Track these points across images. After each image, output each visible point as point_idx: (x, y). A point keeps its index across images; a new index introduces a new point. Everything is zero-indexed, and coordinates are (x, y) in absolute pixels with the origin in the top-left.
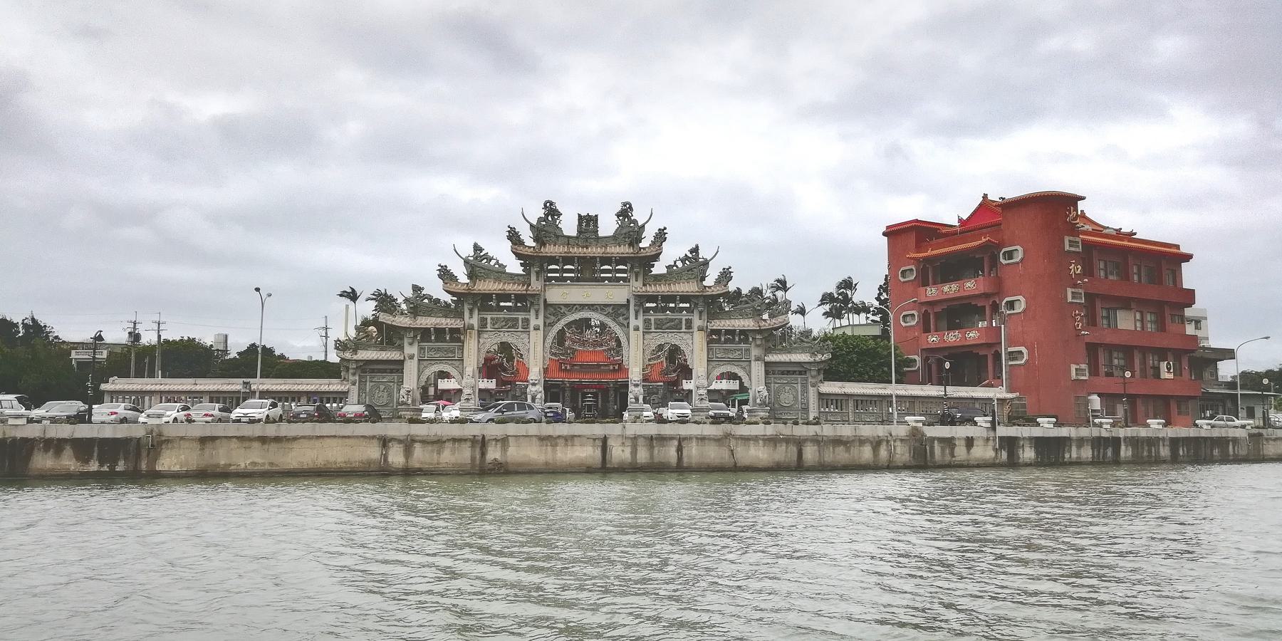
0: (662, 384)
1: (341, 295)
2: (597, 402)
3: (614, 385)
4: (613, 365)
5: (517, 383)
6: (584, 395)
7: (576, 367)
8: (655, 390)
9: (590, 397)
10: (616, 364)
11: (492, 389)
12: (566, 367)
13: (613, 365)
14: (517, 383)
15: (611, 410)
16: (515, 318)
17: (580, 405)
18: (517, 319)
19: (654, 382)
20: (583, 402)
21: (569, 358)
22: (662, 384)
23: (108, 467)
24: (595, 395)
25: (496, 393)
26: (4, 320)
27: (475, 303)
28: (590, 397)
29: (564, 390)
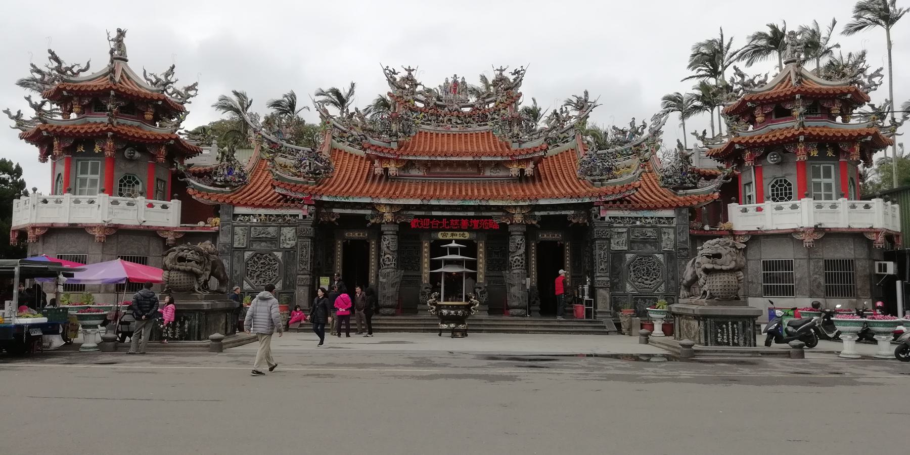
0: (670, 213)
1: (233, 92)
2: (473, 265)
3: (525, 217)
4: (520, 162)
5: (239, 210)
6: (437, 248)
7: (414, 172)
8: (650, 233)
9: (454, 251)
10: (527, 161)
11: (167, 230)
12: (386, 170)
13: (520, 162)
14: (239, 210)
15: (515, 291)
16: (820, 175)
17: (426, 271)
18: (830, 177)
19: (649, 209)
20: (435, 265)
21: (394, 146)
22: (670, 213)
23: (76, 336)
24: (469, 248)
25: (178, 242)
26: (4, 161)
27: (904, 192)
28: (454, 251)
29: (377, 231)
